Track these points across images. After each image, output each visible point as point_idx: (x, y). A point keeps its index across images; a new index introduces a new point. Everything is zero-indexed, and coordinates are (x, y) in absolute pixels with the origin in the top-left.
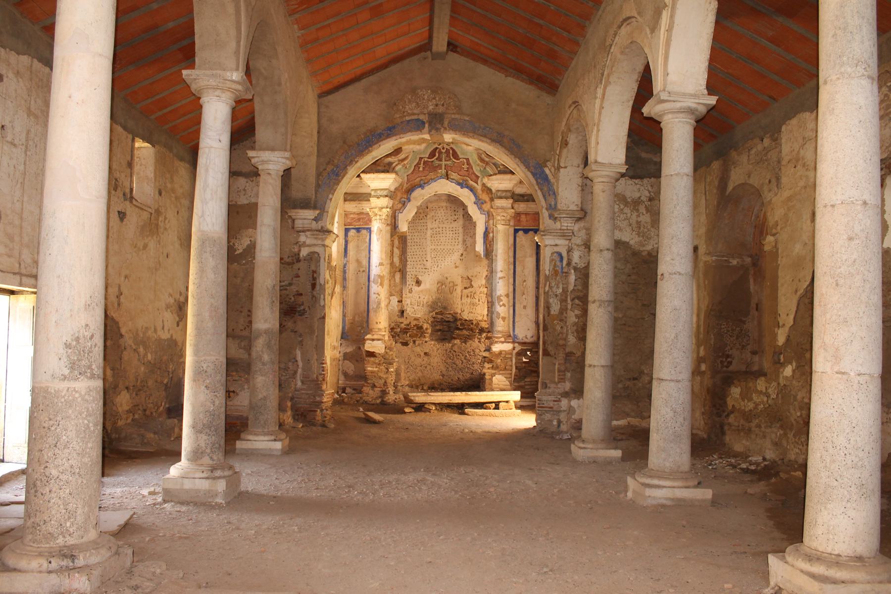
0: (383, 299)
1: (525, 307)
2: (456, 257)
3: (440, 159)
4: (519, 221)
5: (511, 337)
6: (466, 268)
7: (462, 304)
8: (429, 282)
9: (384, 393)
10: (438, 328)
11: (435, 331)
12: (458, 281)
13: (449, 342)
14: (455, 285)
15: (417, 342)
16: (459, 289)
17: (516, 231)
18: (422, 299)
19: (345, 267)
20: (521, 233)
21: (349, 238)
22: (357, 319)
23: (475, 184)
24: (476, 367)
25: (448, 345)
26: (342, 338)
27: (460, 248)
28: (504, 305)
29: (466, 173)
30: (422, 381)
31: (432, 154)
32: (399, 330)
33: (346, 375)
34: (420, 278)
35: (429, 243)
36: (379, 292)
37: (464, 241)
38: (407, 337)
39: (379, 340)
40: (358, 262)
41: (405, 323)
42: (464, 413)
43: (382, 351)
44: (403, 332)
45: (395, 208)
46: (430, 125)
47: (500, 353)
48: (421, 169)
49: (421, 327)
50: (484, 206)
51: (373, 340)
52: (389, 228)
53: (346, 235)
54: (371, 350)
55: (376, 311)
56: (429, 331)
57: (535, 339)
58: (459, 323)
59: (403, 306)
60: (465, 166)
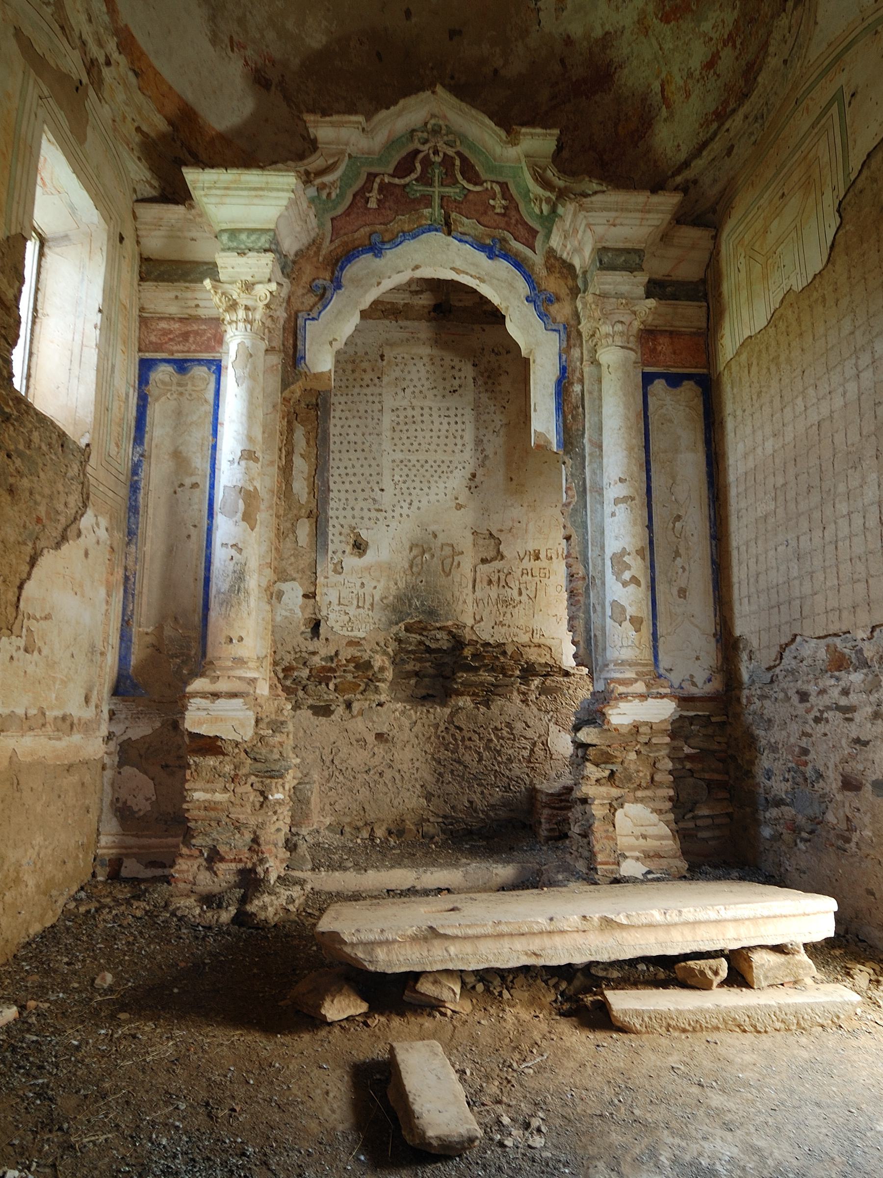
0: (253, 564)
1: (682, 593)
2: (457, 481)
3: (425, 180)
4: (653, 350)
5: (655, 676)
6: (485, 511)
8: (388, 545)
9: (250, 882)
10: (409, 667)
11: (402, 675)
12: (465, 542)
13: (443, 704)
14: (456, 553)
15: (356, 706)
16: (467, 562)
17: (648, 379)
18: (368, 589)
20: (659, 385)
21: (152, 389)
22: (168, 632)
23: (528, 252)
24: (517, 769)
25: (442, 712)
26: (116, 691)
28: (634, 580)
29: (502, 222)
30: (371, 816)
31: (404, 167)
32: (305, 673)
33: (123, 813)
34: (364, 534)
35: (387, 445)
36: (236, 542)
37: (478, 442)
38: (328, 693)
39: (234, 695)
40: (179, 458)
41: (323, 652)
42: (600, 1019)
43: (248, 733)
44: (314, 678)
45: (296, 305)
47: (636, 728)
48: (373, 204)
49: (368, 665)
50: (554, 309)
51: (216, 695)
52: (275, 360)
53: (143, 380)
54: (203, 730)
55: (226, 603)
56: (389, 675)
57: (716, 685)
58: (468, 652)
59: (316, 608)
60: (498, 203)
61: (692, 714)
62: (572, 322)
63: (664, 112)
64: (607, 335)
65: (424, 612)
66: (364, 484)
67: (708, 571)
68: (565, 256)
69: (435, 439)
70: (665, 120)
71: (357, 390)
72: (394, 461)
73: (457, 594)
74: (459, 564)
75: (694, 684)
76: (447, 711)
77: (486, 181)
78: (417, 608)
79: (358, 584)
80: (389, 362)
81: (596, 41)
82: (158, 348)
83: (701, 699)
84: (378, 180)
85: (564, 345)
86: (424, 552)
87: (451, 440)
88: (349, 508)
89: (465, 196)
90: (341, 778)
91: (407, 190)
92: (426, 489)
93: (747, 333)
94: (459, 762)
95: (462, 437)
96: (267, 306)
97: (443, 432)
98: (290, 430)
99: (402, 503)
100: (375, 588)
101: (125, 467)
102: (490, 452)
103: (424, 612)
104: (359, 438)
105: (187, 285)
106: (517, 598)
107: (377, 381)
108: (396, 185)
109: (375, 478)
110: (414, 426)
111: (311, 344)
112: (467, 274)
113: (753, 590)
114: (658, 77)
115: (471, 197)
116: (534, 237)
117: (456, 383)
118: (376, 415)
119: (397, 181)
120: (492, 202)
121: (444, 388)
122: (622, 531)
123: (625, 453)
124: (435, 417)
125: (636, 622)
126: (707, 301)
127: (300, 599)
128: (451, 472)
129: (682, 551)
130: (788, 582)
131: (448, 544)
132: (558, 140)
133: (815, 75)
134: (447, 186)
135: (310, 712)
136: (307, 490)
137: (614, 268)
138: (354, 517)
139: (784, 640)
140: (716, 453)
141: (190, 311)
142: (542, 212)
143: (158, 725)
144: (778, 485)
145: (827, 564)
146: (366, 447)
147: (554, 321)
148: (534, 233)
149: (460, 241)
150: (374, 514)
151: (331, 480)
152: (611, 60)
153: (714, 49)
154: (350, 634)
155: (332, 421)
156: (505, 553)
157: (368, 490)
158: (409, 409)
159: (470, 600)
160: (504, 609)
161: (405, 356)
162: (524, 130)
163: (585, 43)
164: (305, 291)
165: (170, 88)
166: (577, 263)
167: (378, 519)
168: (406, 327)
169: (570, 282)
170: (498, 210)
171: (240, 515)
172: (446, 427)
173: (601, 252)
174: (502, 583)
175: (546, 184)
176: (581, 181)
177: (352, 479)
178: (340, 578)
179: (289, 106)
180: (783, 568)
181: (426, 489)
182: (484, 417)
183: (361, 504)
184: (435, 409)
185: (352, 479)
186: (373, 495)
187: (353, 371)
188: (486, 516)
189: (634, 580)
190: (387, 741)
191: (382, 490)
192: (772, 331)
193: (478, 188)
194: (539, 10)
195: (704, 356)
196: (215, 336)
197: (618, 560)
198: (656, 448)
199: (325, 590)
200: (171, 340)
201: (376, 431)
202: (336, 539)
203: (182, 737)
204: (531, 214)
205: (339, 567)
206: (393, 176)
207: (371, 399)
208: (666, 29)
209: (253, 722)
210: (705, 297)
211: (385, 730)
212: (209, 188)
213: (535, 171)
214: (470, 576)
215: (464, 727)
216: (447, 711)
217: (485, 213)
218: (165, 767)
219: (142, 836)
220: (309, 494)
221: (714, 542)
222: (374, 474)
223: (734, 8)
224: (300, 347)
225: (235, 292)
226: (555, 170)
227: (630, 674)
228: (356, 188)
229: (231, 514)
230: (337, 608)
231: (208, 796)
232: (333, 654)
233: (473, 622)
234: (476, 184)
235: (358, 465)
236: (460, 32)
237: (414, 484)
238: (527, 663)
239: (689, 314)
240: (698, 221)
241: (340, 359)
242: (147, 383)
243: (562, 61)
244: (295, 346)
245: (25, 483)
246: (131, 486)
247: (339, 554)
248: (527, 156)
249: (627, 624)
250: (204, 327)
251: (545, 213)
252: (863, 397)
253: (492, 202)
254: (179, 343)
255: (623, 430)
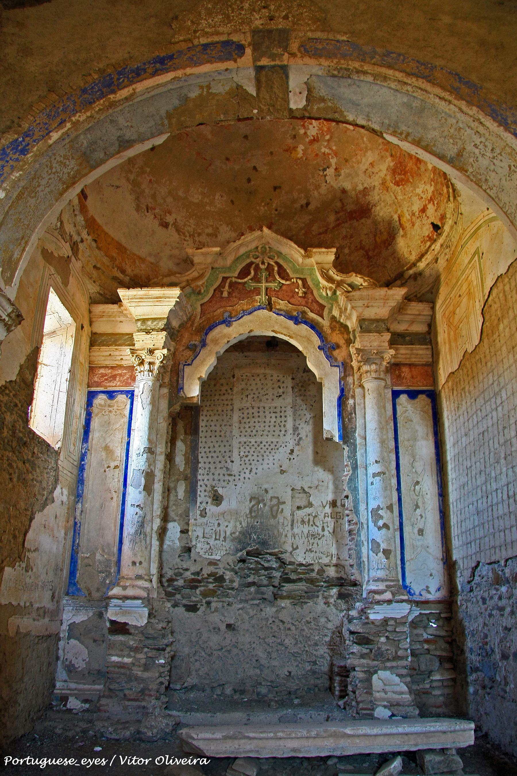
1: (421, 532)
3: (256, 279)
4: (399, 376)
7: (294, 536)
15: (213, 605)
17: (396, 394)
18: (222, 528)
19: (82, 458)
20: (403, 398)
21: (95, 410)
27: (306, 430)
28: (386, 526)
31: (244, 273)
34: (220, 491)
38: (196, 596)
46: (254, 50)
47: (386, 621)
48: (225, 294)
50: (336, 353)
61: (428, 612)
62: (348, 361)
63: (401, 232)
64: (367, 372)
65: (259, 543)
66: (221, 458)
67: (438, 517)
68: (342, 321)
69: (267, 427)
70: (402, 236)
71: (217, 397)
72: (240, 443)
73: (281, 530)
74: (282, 510)
75: (429, 592)
76: (274, 609)
77: (293, 278)
78: (254, 540)
79: (216, 524)
80: (238, 379)
81: (360, 192)
82: (98, 385)
83: (433, 602)
84: (228, 281)
85: (343, 375)
86: (259, 503)
87: (277, 428)
88: (211, 474)
89: (281, 287)
90: (203, 653)
91: (246, 285)
92: (261, 461)
93: (450, 371)
94: (281, 644)
95: (284, 426)
96: (162, 362)
97: (272, 423)
98: (172, 441)
99: (245, 470)
100: (227, 526)
101: (76, 457)
102: (303, 435)
103: (259, 543)
104: (218, 428)
105: (116, 347)
106: (322, 533)
107: (229, 391)
108: (240, 283)
109: (228, 454)
110: (254, 420)
111: (187, 380)
112: (282, 333)
113: (459, 531)
114: (396, 213)
115: (284, 288)
116: (323, 310)
117: (281, 391)
118: (229, 413)
119: (240, 281)
120: (297, 290)
121: (273, 394)
122: (378, 495)
123: (378, 445)
124: (267, 413)
125: (387, 553)
126: (431, 345)
127: (179, 534)
128: (278, 449)
129: (420, 504)
130: (474, 527)
131: (275, 497)
132: (336, 254)
133: (467, 237)
134: (270, 282)
135: (183, 609)
136: (184, 462)
137: (369, 331)
138: (214, 480)
139: (474, 565)
140: (441, 440)
141: (117, 363)
142: (327, 295)
143: (91, 614)
144: (468, 467)
145: (489, 519)
146: (222, 433)
147: (336, 360)
148: (323, 307)
149: (278, 314)
150: (227, 478)
151: (200, 456)
152: (369, 202)
153: (424, 203)
154: (210, 557)
155: (201, 418)
156: (313, 503)
157: (223, 462)
158: (250, 409)
159: (289, 535)
160: (313, 541)
161: (248, 374)
162: (314, 250)
163: (353, 192)
164: (184, 348)
165: (113, 239)
166: (349, 324)
167: (229, 481)
168: (249, 356)
169: (346, 336)
170: (300, 295)
171: (142, 487)
172: (274, 419)
173: (361, 321)
174: (311, 523)
175: (330, 279)
176: (351, 276)
177: (213, 454)
178: (204, 520)
179: (179, 234)
180: (472, 519)
181: (261, 461)
182: (298, 413)
183: (219, 471)
184: (267, 408)
185: (213, 454)
186: (226, 465)
187: (215, 385)
188: (300, 478)
189: (386, 526)
190: (234, 629)
191: (232, 462)
192: (461, 371)
193: (288, 283)
194: (325, 176)
195: (431, 379)
196: (131, 376)
197: (376, 513)
198: (402, 438)
199: (195, 528)
200: (106, 379)
201: (229, 424)
202: (202, 494)
203: (105, 622)
204: (321, 296)
205: (203, 513)
206: (238, 277)
207: (226, 403)
208: (398, 189)
209: (147, 615)
210: (430, 342)
211: (232, 622)
212: (132, 299)
213: (322, 272)
214: (290, 518)
215: (285, 620)
216: (274, 609)
217: (293, 296)
218: (95, 641)
219: (80, 683)
220: (185, 464)
221: (441, 498)
222: (227, 451)
223: (431, 185)
224: (180, 382)
225: (144, 354)
226: (334, 271)
227: (381, 586)
228: (215, 286)
229: (137, 487)
230: (203, 540)
231: (120, 659)
232: (199, 570)
233: (291, 549)
234: (287, 280)
235: (217, 446)
236: (280, 188)
237: (253, 458)
238: (328, 577)
239: (421, 353)
240: (420, 299)
241: (205, 385)
242: (92, 406)
243: (341, 200)
244: (178, 381)
245: (30, 476)
246: (80, 468)
247: (204, 504)
248: (317, 263)
249: (381, 554)
250: (125, 371)
251: (329, 295)
252: (499, 422)
253: (297, 290)
254: (111, 381)
255: (377, 430)
